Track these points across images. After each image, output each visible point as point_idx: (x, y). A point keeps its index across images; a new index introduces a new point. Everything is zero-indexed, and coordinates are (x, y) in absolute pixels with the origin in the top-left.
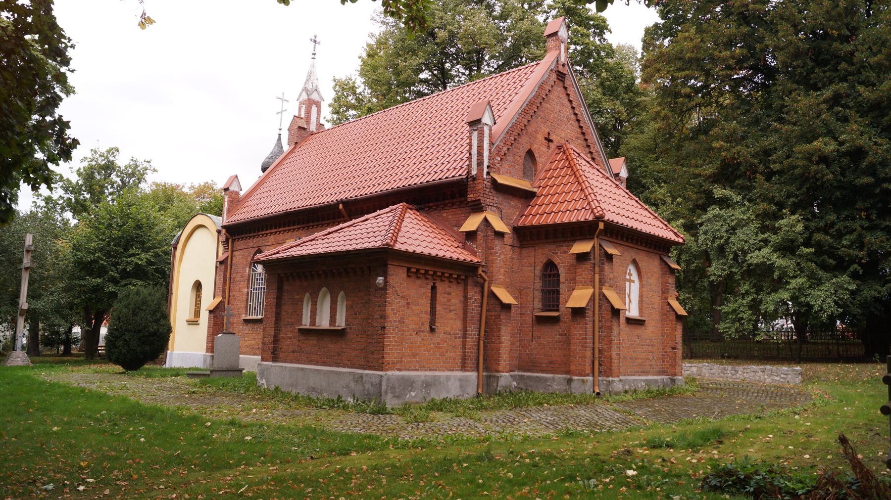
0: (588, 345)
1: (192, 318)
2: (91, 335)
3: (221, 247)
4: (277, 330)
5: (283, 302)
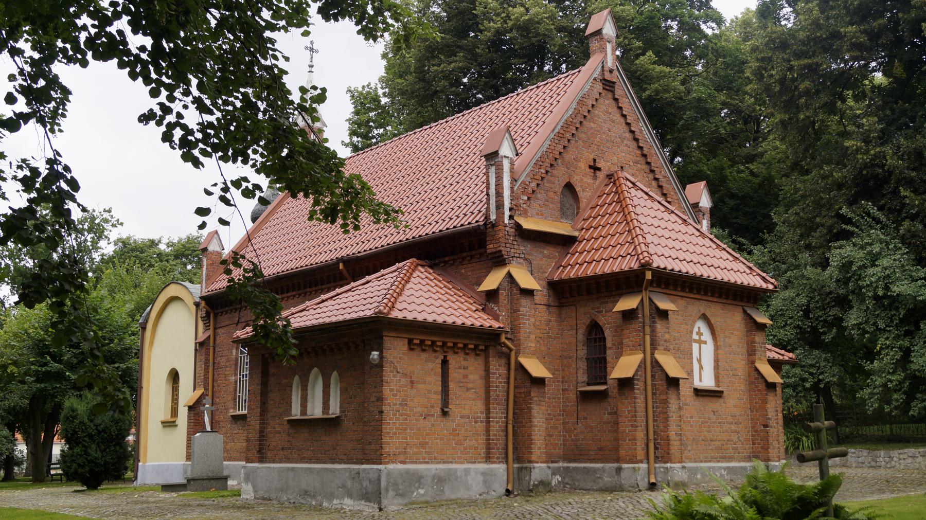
0: (639, 424)
1: (168, 417)
2: (40, 451)
3: (201, 325)
4: (263, 423)
5: (269, 389)
